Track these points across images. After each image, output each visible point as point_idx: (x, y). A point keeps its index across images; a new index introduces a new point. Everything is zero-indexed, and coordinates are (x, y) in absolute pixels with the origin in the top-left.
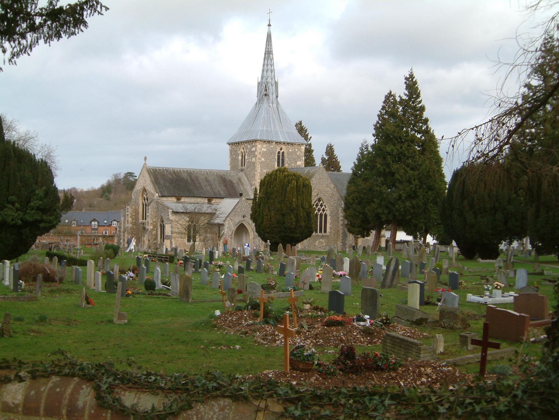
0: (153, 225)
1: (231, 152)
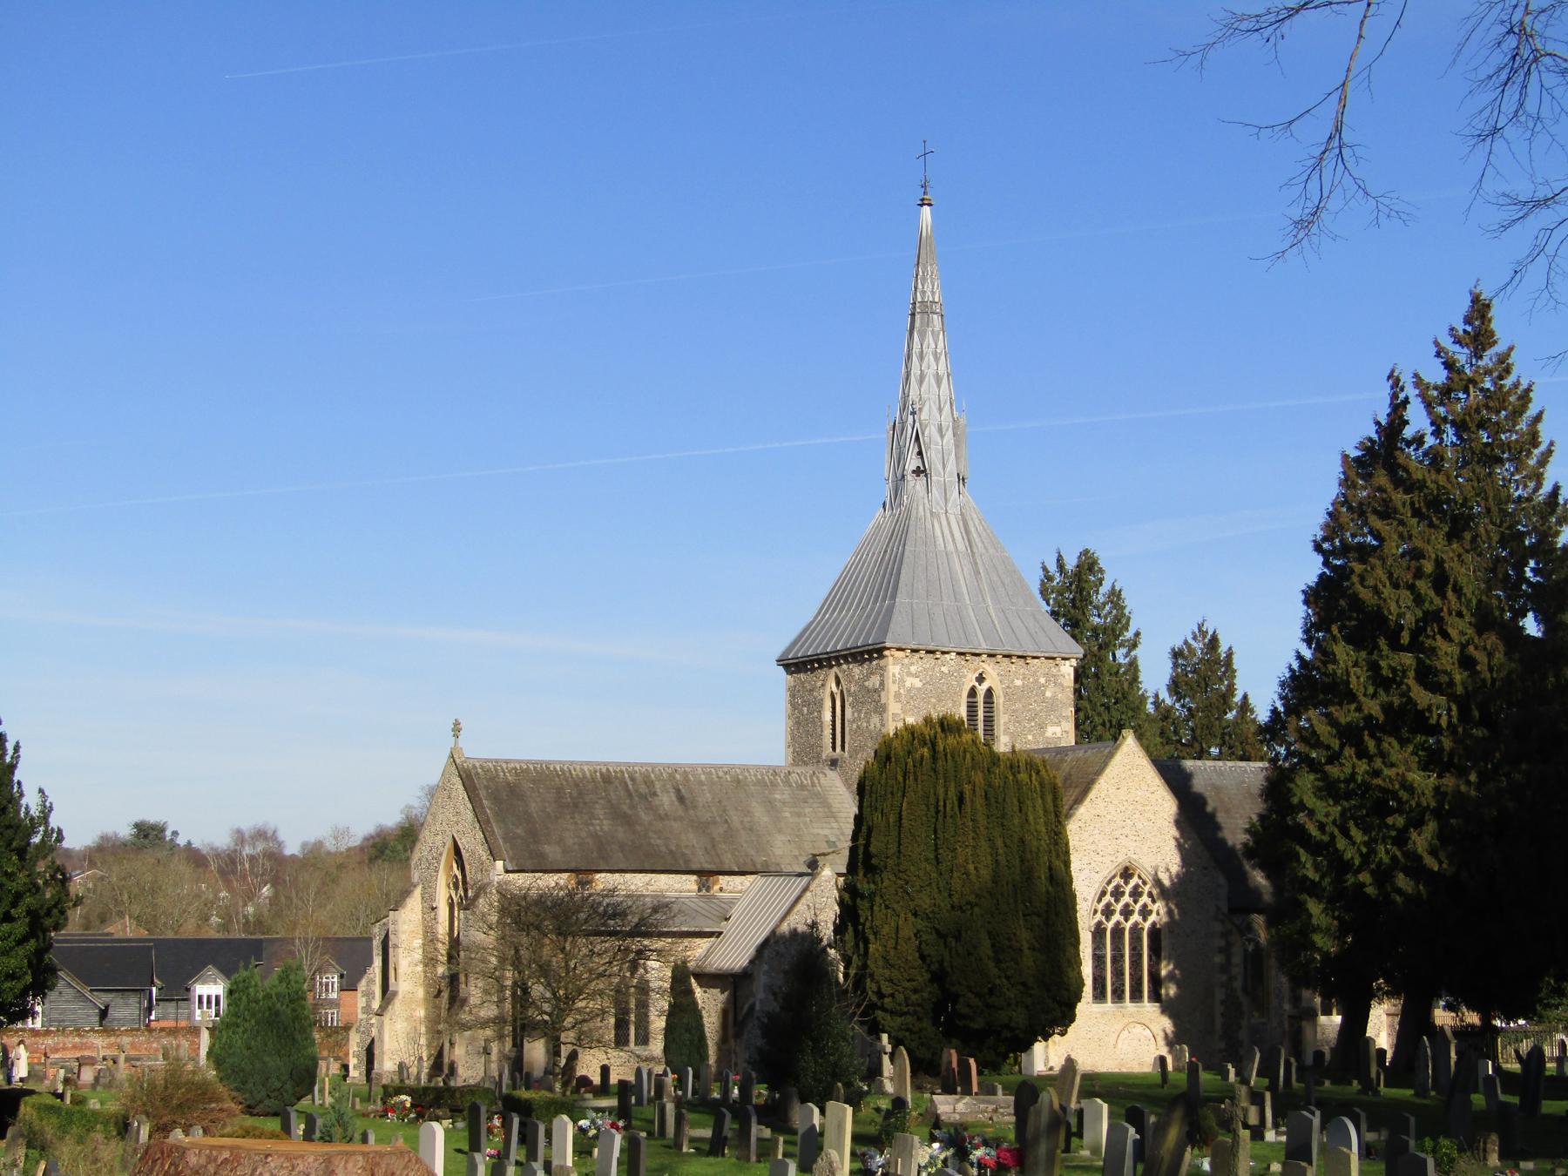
1: (793, 696)
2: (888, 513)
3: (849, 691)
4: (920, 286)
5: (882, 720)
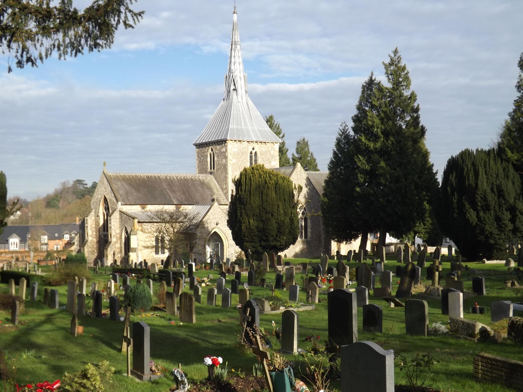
0: (117, 238)
1: (198, 154)
2: (225, 101)
3: (216, 152)
4: (234, 37)
5: (226, 161)
